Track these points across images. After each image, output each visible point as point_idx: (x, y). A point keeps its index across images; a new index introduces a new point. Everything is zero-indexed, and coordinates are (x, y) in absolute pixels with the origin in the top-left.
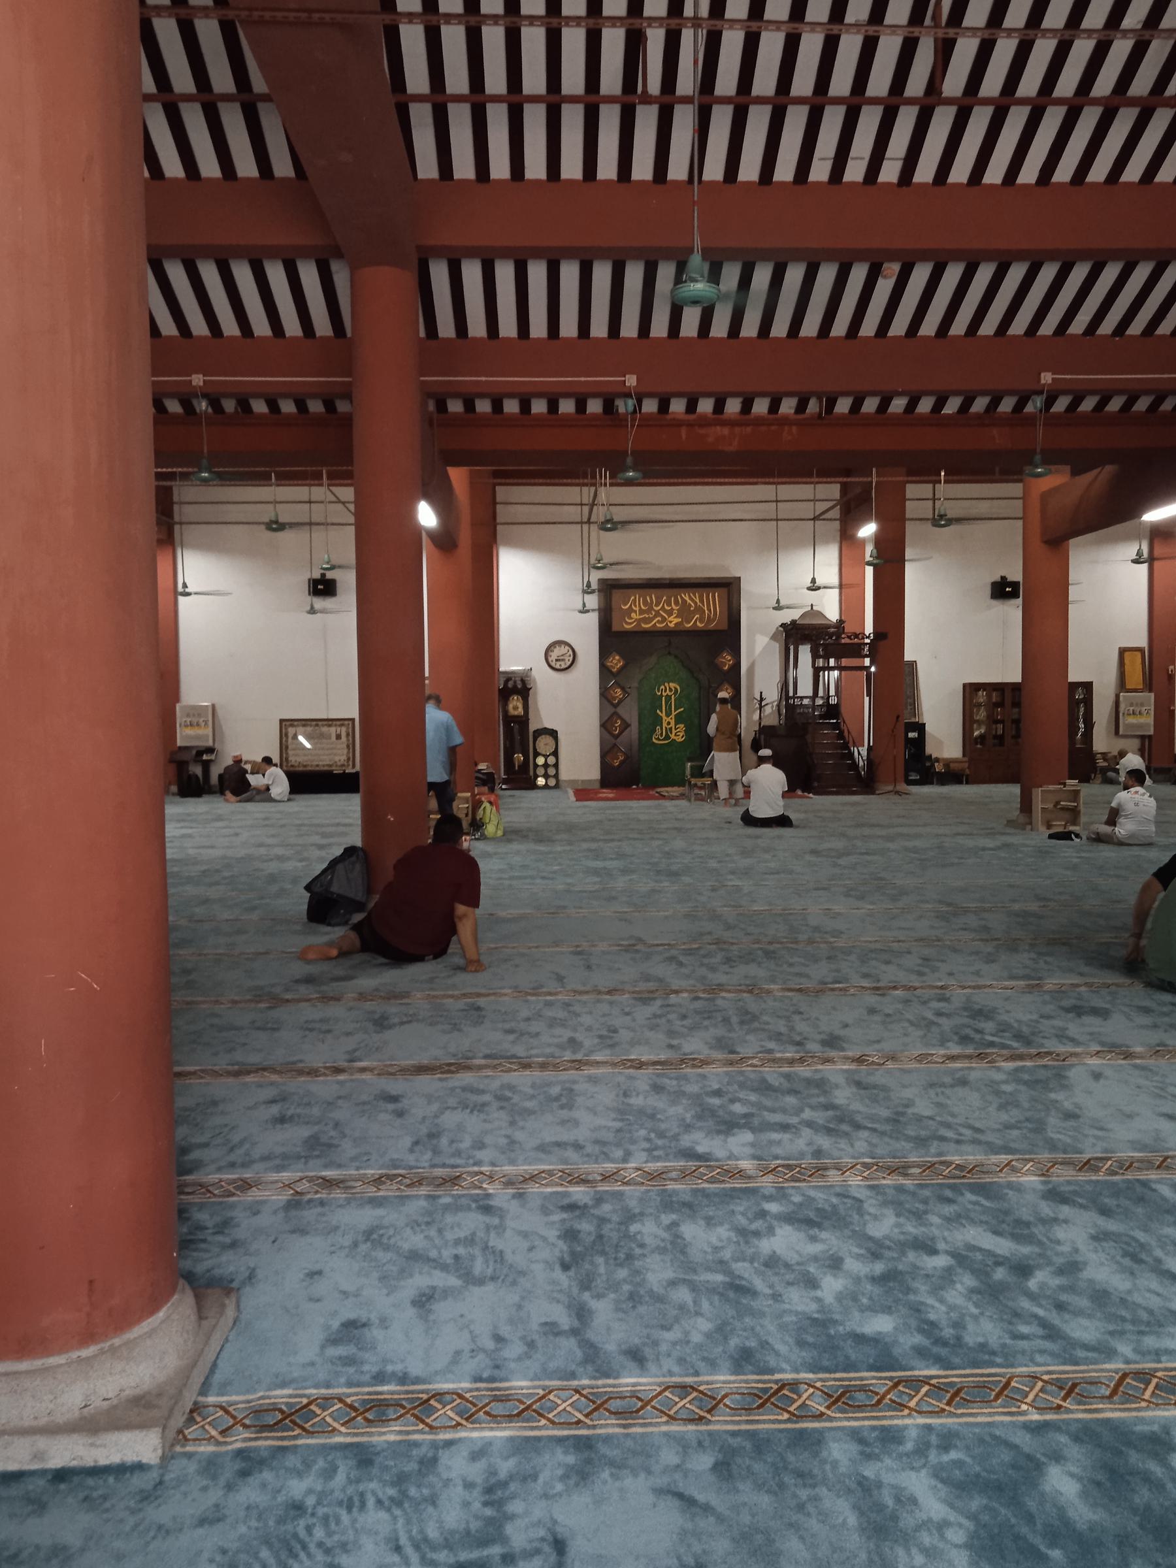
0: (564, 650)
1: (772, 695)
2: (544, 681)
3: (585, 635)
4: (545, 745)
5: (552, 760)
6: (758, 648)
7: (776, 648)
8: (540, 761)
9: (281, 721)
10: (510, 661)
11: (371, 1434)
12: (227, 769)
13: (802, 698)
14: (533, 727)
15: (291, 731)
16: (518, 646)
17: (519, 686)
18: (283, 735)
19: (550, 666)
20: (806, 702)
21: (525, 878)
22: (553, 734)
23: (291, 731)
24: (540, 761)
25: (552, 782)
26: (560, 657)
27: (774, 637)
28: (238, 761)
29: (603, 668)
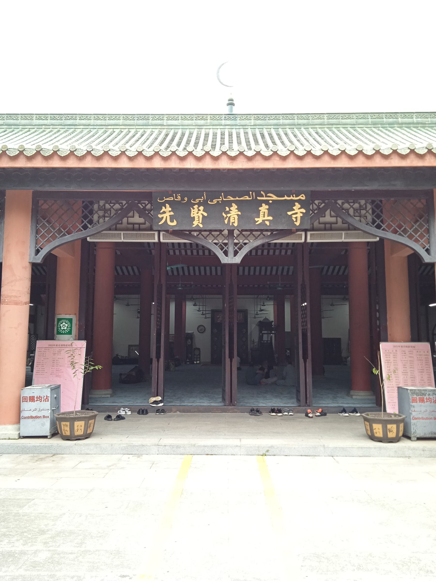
0: (202, 327)
1: (256, 340)
2: (197, 334)
3: (207, 323)
4: (197, 352)
5: (198, 356)
6: (252, 327)
7: (257, 328)
8: (195, 356)
9: (130, 346)
10: (188, 330)
11: (305, 358)
12: (114, 357)
13: (264, 341)
14: (194, 347)
15: (131, 348)
16: (190, 327)
17: (190, 336)
18: (129, 349)
19: (199, 332)
20: (265, 342)
21: (68, 140)
22: (199, 349)
23: (131, 348)
24: (195, 356)
25: (198, 359)
26: (201, 329)
27: (257, 325)
28: (117, 355)
29: (212, 332)
